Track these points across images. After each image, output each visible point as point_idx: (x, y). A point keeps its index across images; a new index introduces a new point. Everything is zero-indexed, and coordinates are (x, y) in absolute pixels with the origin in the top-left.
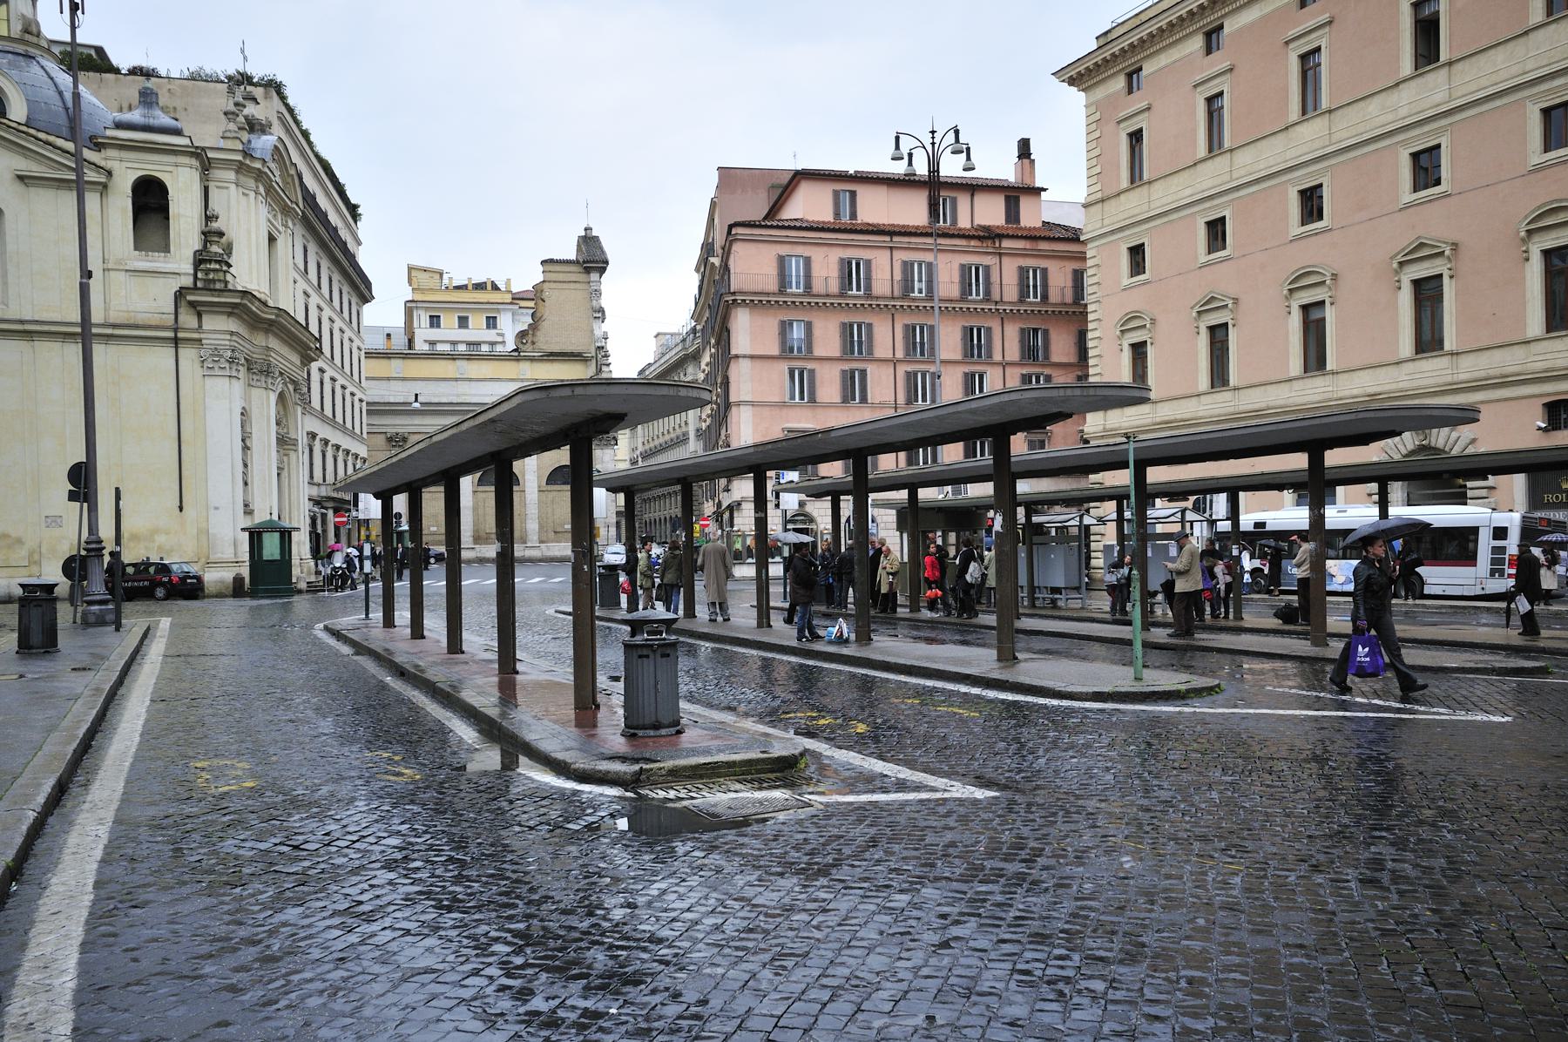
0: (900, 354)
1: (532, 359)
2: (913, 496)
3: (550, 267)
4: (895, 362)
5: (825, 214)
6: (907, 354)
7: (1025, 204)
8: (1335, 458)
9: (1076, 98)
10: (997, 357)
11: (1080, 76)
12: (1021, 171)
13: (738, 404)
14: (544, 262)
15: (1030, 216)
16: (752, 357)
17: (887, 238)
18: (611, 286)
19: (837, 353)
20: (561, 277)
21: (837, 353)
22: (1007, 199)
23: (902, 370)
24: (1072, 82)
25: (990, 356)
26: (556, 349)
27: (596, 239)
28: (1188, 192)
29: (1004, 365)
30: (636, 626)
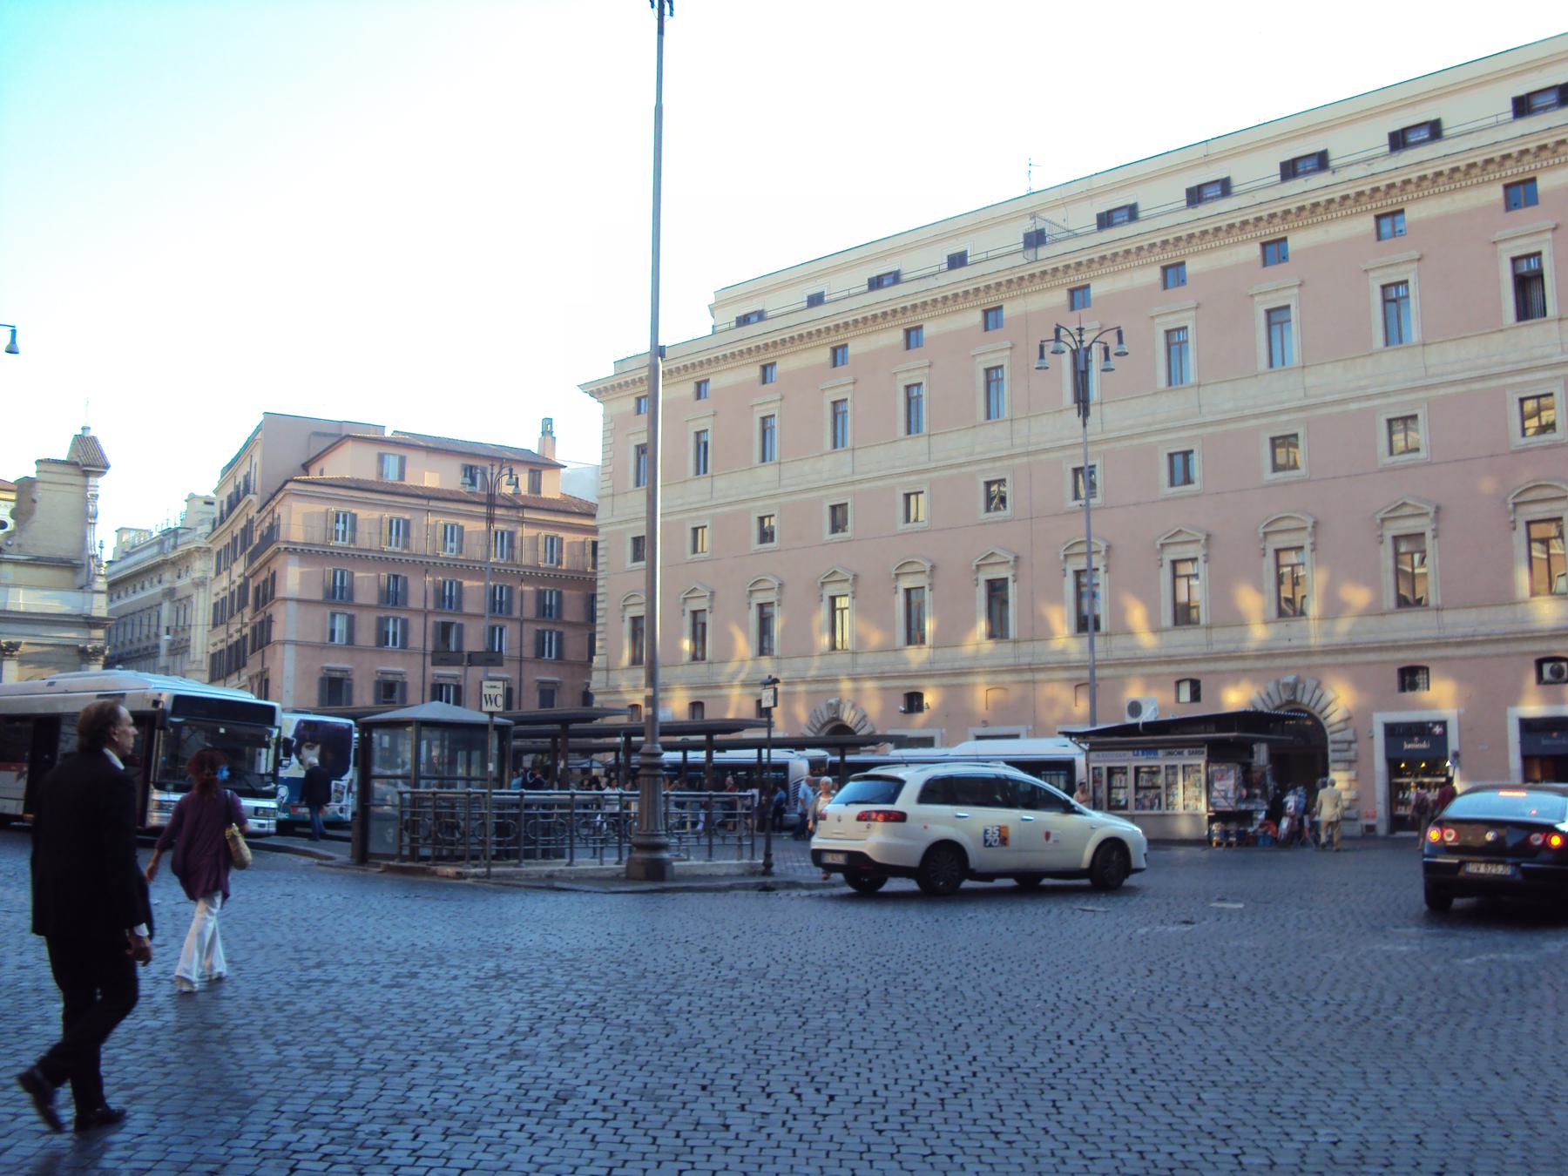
0: (430, 606)
1: (16, 563)
2: (709, 756)
3: (44, 467)
4: (426, 614)
5: (368, 473)
6: (437, 606)
7: (546, 476)
8: (717, 737)
9: (596, 409)
10: (516, 614)
11: (598, 391)
12: (542, 443)
13: (284, 643)
14: (39, 462)
15: (552, 488)
16: (299, 601)
17: (425, 502)
18: (103, 486)
19: (375, 602)
20: (56, 478)
21: (375, 602)
22: (531, 471)
23: (431, 620)
24: (592, 394)
25: (510, 612)
26: (43, 553)
27: (94, 440)
28: (680, 501)
29: (522, 621)
30: (1533, 594)
